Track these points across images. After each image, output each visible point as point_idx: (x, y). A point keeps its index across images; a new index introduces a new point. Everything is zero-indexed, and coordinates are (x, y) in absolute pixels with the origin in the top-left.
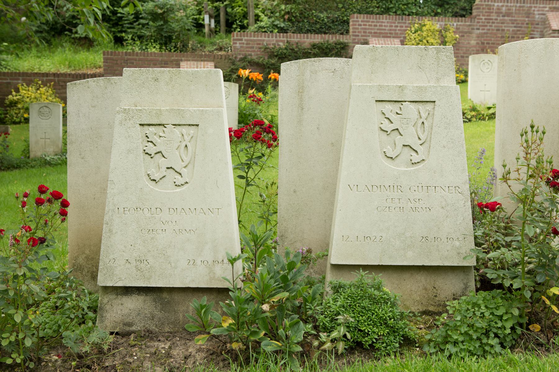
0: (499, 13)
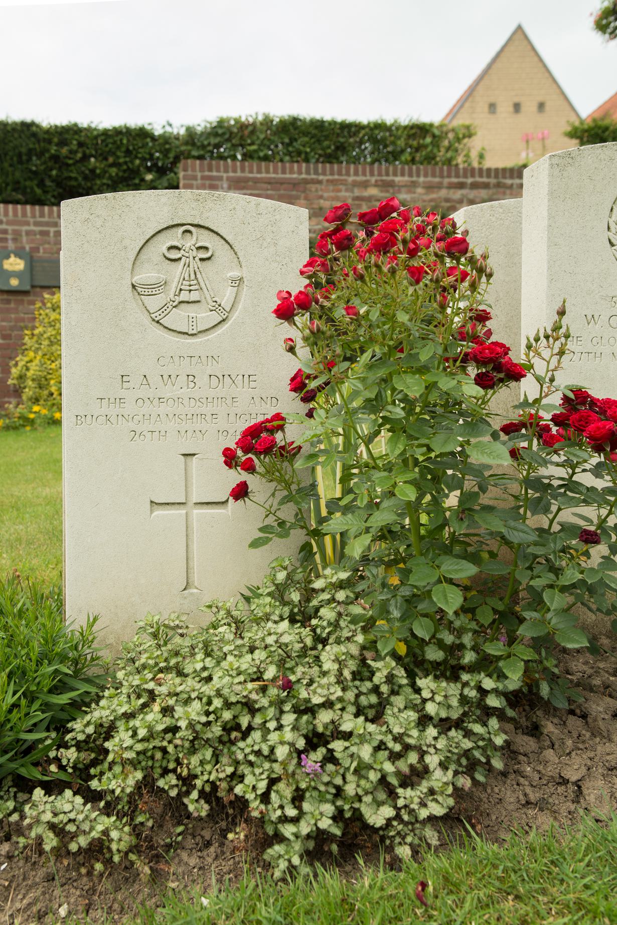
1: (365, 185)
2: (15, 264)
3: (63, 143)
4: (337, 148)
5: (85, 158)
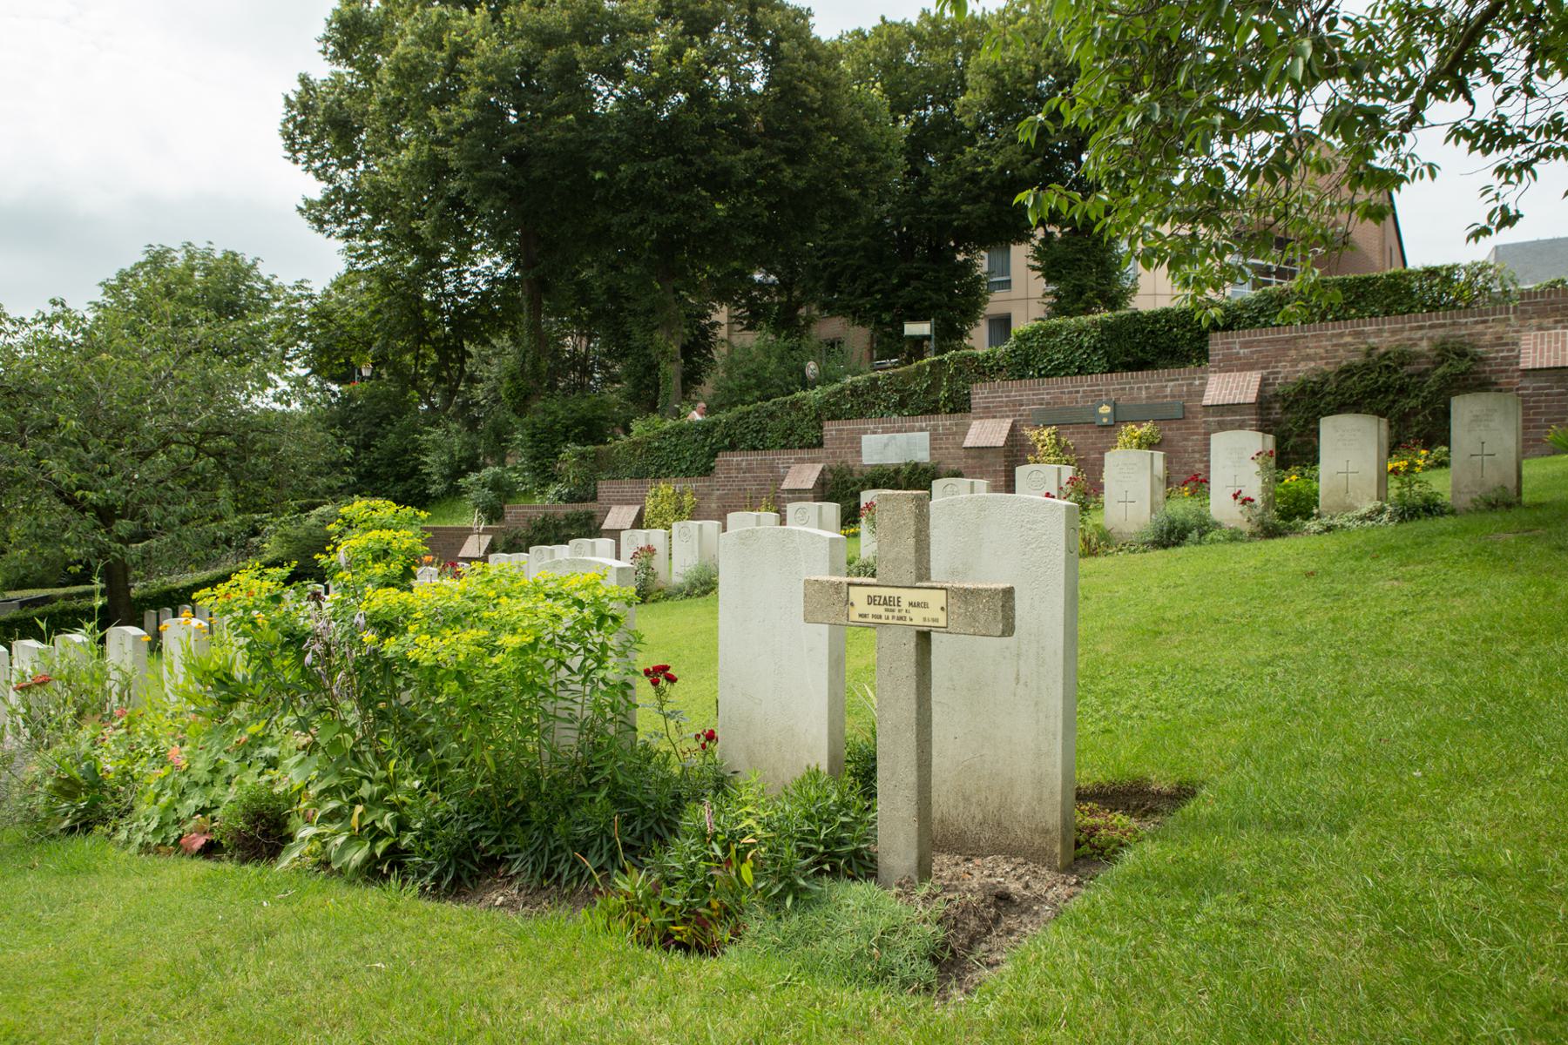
0: (739, 469)
1: (1341, 335)
2: (1105, 409)
3: (1158, 321)
4: (1358, 297)
5: (1171, 329)
